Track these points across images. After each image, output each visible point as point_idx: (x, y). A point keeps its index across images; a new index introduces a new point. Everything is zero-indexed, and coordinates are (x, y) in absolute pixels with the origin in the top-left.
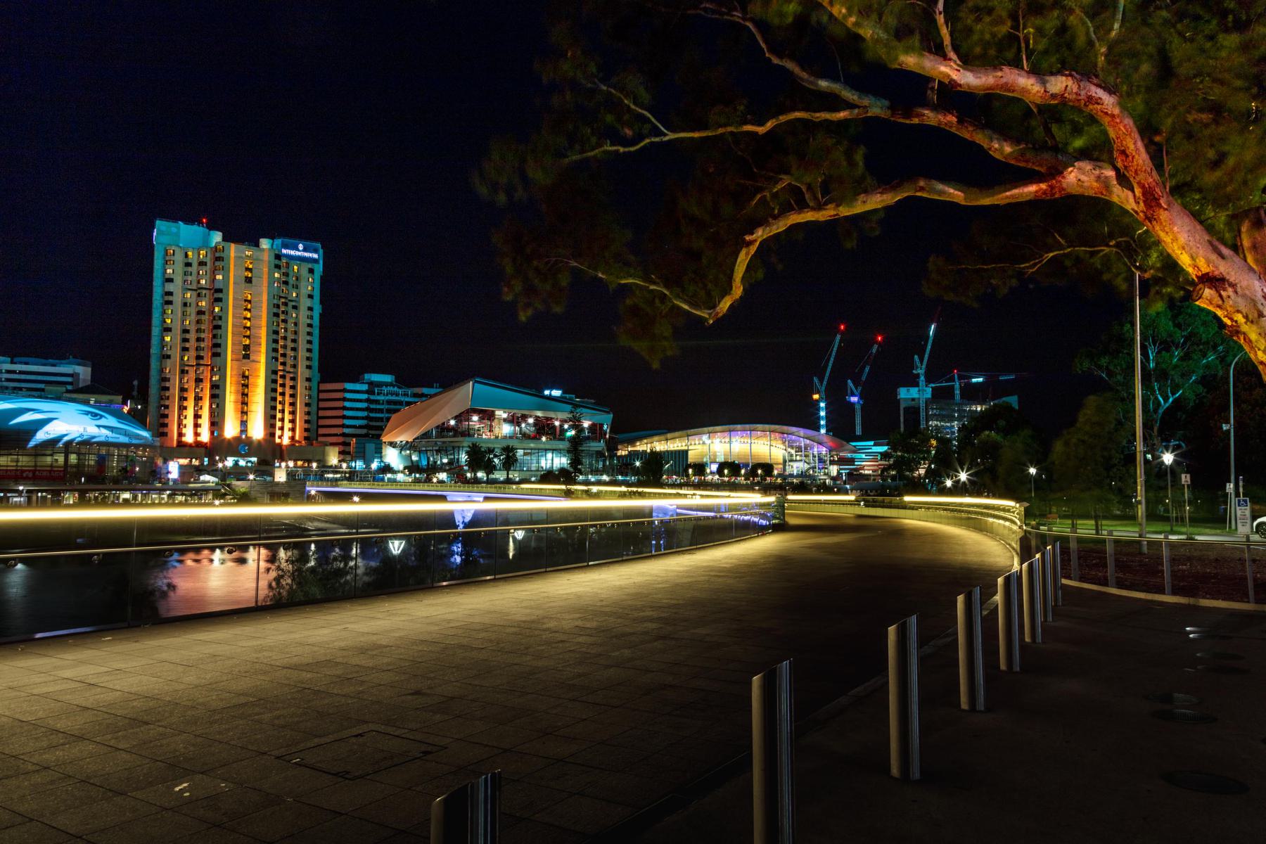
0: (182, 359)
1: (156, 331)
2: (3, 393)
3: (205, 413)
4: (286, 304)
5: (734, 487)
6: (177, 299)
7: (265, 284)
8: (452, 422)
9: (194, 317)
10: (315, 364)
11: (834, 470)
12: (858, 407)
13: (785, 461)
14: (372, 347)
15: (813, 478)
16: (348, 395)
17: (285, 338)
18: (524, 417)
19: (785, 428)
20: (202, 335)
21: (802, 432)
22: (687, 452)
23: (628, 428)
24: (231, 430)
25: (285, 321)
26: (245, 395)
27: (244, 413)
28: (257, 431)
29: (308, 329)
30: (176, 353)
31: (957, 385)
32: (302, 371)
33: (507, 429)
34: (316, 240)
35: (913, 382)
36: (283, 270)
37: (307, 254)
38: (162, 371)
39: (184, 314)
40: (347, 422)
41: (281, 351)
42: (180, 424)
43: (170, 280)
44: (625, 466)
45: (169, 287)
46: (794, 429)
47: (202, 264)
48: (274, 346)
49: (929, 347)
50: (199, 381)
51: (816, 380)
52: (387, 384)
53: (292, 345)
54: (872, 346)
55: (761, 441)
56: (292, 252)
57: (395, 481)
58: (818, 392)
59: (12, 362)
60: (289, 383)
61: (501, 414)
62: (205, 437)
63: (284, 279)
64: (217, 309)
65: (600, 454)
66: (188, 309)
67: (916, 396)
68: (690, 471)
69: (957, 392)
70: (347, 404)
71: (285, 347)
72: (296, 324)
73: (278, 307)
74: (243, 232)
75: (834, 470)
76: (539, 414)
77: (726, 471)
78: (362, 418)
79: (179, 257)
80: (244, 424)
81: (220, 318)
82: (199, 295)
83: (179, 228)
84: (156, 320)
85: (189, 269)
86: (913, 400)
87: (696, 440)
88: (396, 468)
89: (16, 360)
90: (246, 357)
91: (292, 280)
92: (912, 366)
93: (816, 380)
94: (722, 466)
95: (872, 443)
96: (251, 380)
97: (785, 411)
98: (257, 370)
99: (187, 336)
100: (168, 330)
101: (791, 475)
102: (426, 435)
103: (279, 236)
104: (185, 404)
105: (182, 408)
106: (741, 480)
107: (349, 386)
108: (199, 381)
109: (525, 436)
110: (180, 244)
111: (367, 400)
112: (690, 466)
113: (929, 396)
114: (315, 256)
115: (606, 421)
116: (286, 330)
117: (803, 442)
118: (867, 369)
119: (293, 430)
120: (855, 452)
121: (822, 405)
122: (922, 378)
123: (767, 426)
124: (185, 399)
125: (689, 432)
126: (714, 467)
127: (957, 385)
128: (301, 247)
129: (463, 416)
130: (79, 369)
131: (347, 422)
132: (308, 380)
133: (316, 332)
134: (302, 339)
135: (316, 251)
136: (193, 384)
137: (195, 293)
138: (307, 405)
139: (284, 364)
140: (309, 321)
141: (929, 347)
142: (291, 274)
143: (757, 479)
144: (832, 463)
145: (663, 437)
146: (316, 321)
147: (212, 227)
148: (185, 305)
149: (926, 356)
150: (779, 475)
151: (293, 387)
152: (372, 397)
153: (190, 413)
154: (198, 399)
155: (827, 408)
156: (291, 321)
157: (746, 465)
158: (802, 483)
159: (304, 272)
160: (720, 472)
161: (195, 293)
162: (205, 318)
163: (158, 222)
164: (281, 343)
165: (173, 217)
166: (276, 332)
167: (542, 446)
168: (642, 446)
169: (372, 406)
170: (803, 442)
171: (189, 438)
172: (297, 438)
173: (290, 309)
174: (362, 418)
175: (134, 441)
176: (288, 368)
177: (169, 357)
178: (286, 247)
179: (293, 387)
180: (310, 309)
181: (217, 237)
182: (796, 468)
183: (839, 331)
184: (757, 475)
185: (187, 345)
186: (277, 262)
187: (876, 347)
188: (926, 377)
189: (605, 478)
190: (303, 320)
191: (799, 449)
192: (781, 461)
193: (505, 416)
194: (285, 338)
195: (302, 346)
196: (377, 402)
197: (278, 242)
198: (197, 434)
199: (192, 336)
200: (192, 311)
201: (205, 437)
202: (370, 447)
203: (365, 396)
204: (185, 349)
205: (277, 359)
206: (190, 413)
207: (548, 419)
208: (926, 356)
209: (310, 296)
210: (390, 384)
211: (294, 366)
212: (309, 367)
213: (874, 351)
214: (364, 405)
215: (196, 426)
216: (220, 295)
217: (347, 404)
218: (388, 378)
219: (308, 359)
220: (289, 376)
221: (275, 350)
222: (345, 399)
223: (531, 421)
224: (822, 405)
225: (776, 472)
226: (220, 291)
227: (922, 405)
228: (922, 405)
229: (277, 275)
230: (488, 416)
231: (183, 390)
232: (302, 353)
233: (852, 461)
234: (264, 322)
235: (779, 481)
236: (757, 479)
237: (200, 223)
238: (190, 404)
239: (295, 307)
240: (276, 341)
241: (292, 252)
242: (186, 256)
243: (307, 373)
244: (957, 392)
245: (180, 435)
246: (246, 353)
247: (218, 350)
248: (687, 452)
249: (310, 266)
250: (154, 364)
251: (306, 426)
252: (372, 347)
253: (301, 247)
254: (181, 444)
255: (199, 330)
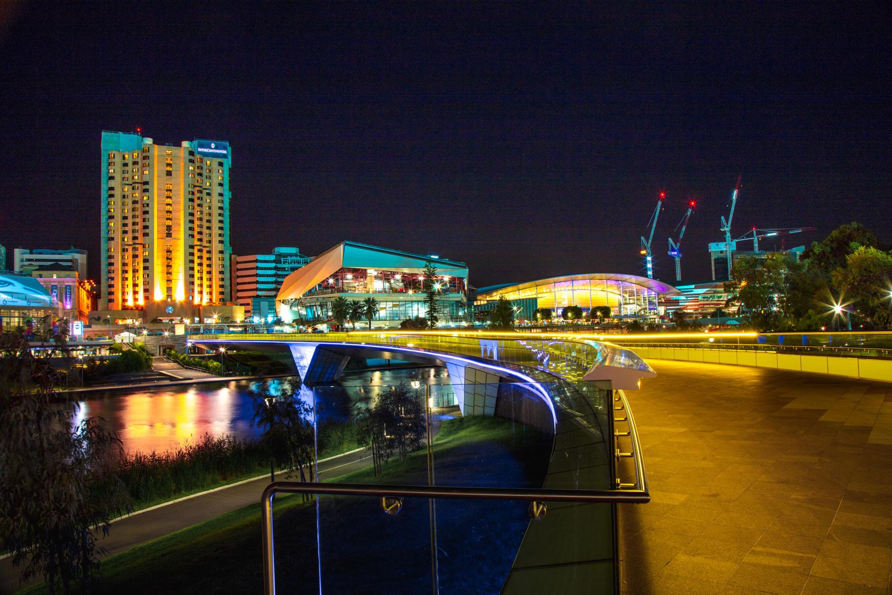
0: (123, 240)
1: (104, 219)
2: (890, 341)
3: (140, 282)
4: (201, 192)
5: (577, 328)
6: (117, 193)
7: (182, 176)
8: (331, 281)
9: (130, 206)
10: (227, 239)
11: (662, 310)
12: (677, 259)
13: (620, 305)
14: (267, 222)
15: (644, 318)
16: (260, 265)
17: (201, 219)
18: (393, 274)
19: (619, 276)
20: (137, 220)
21: (633, 278)
22: (536, 299)
23: (482, 280)
24: (159, 295)
25: (199, 205)
26: (169, 266)
27: (169, 281)
28: (180, 295)
29: (220, 211)
30: (118, 236)
31: (756, 240)
32: (216, 246)
33: (379, 285)
34: (223, 139)
35: (721, 238)
36: (198, 164)
37: (218, 151)
38: (109, 250)
39: (123, 204)
40: (259, 286)
41: (197, 229)
42: (123, 293)
43: (112, 178)
44: (482, 314)
45: (112, 183)
46: (627, 277)
47: (135, 163)
48: (191, 225)
49: (733, 209)
50: (135, 256)
51: (643, 238)
52: (291, 255)
53: (208, 224)
54: (686, 211)
55: (600, 288)
56: (206, 150)
57: (282, 332)
58: (645, 248)
59: (31, 253)
60: (205, 255)
61: (372, 272)
62: (141, 302)
63: (198, 171)
64: (145, 198)
65: (459, 305)
66: (126, 200)
67: (724, 249)
68: (539, 315)
69: (756, 245)
70: (260, 272)
71: (201, 226)
72: (210, 208)
73: (193, 193)
74: (168, 136)
75: (662, 310)
76: (406, 270)
77: (570, 315)
78: (272, 283)
79: (118, 160)
80: (169, 289)
81: (148, 205)
82: (133, 188)
83: (119, 137)
84: (103, 211)
85: (126, 168)
86: (722, 252)
87: (544, 289)
88: (286, 322)
89: (34, 251)
90: (169, 235)
91: (205, 173)
92: (720, 225)
93: (643, 238)
94: (566, 311)
95: (693, 286)
96: (174, 254)
97: (619, 262)
98: (177, 245)
99: (126, 221)
100: (111, 217)
101: (626, 316)
102: (310, 292)
103: (196, 139)
104: (126, 275)
105: (125, 279)
106: (582, 322)
107: (260, 257)
108: (135, 256)
109: (394, 291)
110: (118, 147)
111: (276, 268)
112: (538, 311)
113: (734, 248)
114: (225, 152)
115: (464, 273)
116: (202, 213)
117: (635, 288)
118: (684, 229)
119: (211, 293)
120: (679, 294)
121: (649, 258)
122: (728, 234)
123: (604, 275)
124: (126, 272)
125: (538, 282)
126: (560, 312)
127: (756, 240)
128: (213, 145)
129: (338, 275)
130: (77, 256)
131: (259, 286)
132: (221, 252)
133: (227, 213)
134: (215, 219)
135: (225, 148)
136: (131, 259)
137: (131, 187)
138: (221, 272)
139: (200, 240)
140: (220, 205)
141: (733, 209)
142: (205, 167)
143: (597, 320)
144: (660, 304)
145: (515, 288)
146: (227, 205)
147: (144, 135)
148: (124, 197)
149: (731, 216)
150: (616, 316)
151: (209, 259)
152: (279, 266)
153: (130, 283)
154: (135, 271)
155: (646, 262)
156: (206, 205)
157: (587, 309)
158: (635, 322)
159: (215, 166)
160: (564, 315)
161: (131, 187)
162: (138, 206)
163: (103, 134)
164: (197, 223)
165: (115, 129)
166: (192, 214)
167: (409, 299)
168: (496, 296)
169: (279, 273)
170: (635, 288)
171: (130, 303)
172: (214, 301)
173: (204, 195)
174: (272, 283)
175: (32, 305)
176: (204, 244)
177: (113, 239)
178: (201, 146)
179: (209, 259)
180: (221, 195)
181: (149, 141)
182: (631, 309)
183: (660, 198)
184: (596, 317)
185: (126, 229)
186: (191, 157)
187: (690, 210)
188: (731, 231)
189: (464, 324)
190: (216, 204)
191: (631, 294)
192: (617, 304)
193: (375, 273)
194: (201, 219)
195: (215, 225)
196: (283, 269)
197: (196, 142)
198: (136, 300)
199: (130, 221)
200: (129, 201)
201: (141, 302)
202: (264, 304)
203: (273, 265)
204: (125, 232)
205: (193, 236)
206: (130, 283)
207: (413, 275)
208: (731, 216)
209: (221, 185)
210: (296, 255)
211: (210, 242)
212: (221, 242)
213: (689, 214)
214: (273, 272)
215: (135, 293)
216: (147, 187)
217: (260, 272)
218: (294, 250)
219: (220, 235)
220: (205, 250)
221: (191, 229)
222: (257, 268)
223: (398, 277)
224: (649, 258)
225: (612, 314)
226: (146, 183)
227: (729, 256)
228: (729, 256)
229: (191, 168)
230: (360, 274)
231: (124, 265)
232: (216, 231)
233: (677, 302)
234: (182, 207)
235: (616, 321)
236: (597, 320)
237: (135, 132)
238: (130, 275)
239: (209, 194)
240: (192, 222)
241: (206, 150)
242: (124, 158)
243: (220, 247)
244: (756, 245)
245: (124, 300)
246: (169, 232)
247: (147, 231)
248: (536, 299)
249: (219, 160)
250: (104, 246)
251: (221, 290)
252: (267, 222)
253: (213, 145)
254: (125, 308)
255: (134, 217)
